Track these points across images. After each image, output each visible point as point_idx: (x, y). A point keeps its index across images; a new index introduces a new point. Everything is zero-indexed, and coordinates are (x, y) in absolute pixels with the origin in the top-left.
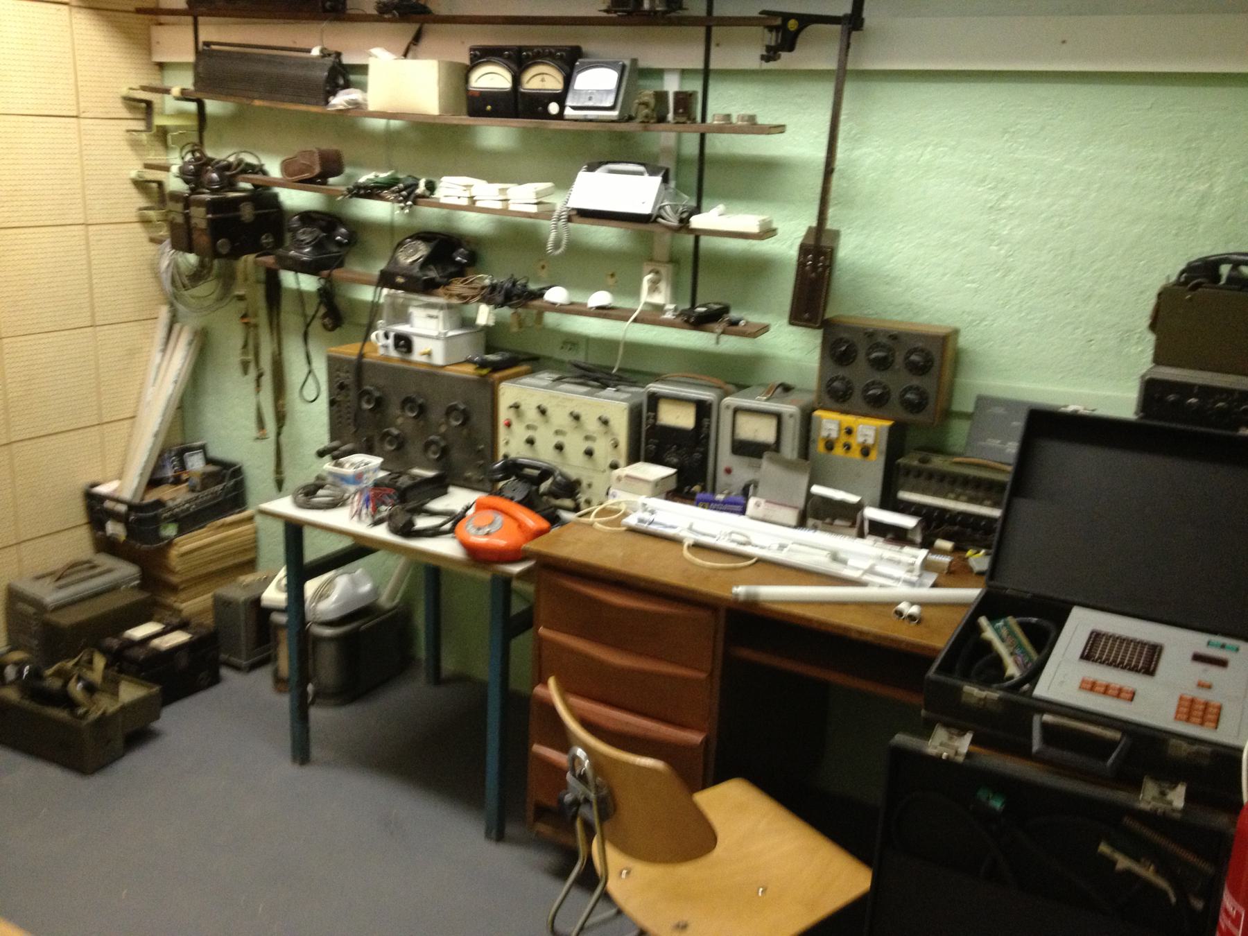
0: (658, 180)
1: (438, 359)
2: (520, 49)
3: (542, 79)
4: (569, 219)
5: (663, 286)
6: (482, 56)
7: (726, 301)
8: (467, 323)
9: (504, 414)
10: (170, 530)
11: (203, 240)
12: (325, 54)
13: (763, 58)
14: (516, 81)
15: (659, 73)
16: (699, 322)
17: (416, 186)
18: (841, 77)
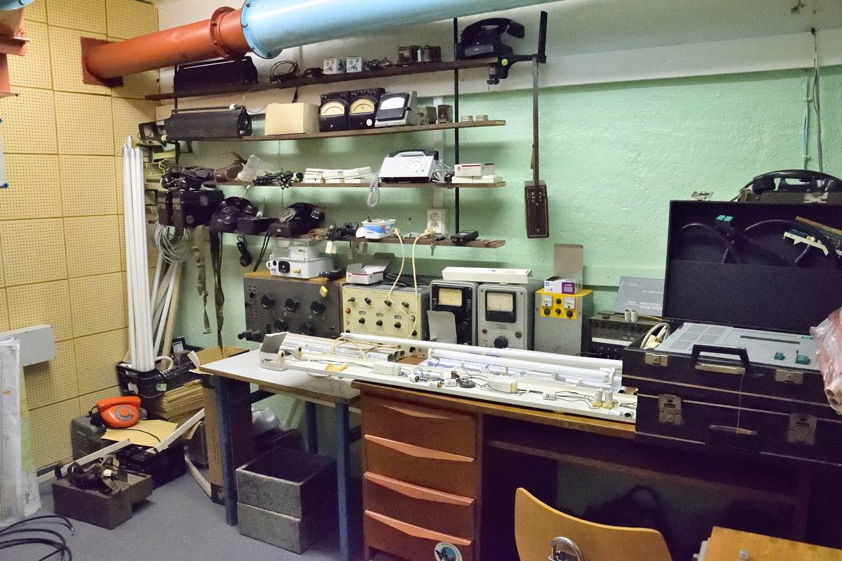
0: (432, 157)
1: (305, 275)
2: (349, 93)
3: (362, 107)
4: (379, 185)
5: (440, 223)
6: (324, 101)
7: (476, 229)
8: (322, 255)
9: (346, 305)
10: (162, 387)
11: (178, 216)
12: (237, 108)
13: (490, 82)
14: (347, 110)
15: (431, 99)
16: (459, 242)
17: (292, 175)
18: (536, 93)
